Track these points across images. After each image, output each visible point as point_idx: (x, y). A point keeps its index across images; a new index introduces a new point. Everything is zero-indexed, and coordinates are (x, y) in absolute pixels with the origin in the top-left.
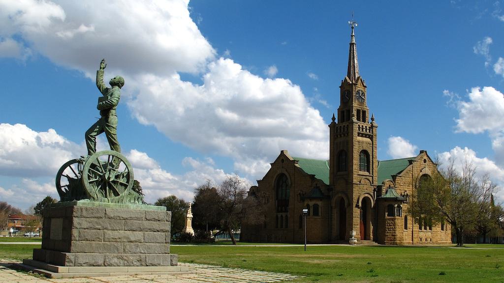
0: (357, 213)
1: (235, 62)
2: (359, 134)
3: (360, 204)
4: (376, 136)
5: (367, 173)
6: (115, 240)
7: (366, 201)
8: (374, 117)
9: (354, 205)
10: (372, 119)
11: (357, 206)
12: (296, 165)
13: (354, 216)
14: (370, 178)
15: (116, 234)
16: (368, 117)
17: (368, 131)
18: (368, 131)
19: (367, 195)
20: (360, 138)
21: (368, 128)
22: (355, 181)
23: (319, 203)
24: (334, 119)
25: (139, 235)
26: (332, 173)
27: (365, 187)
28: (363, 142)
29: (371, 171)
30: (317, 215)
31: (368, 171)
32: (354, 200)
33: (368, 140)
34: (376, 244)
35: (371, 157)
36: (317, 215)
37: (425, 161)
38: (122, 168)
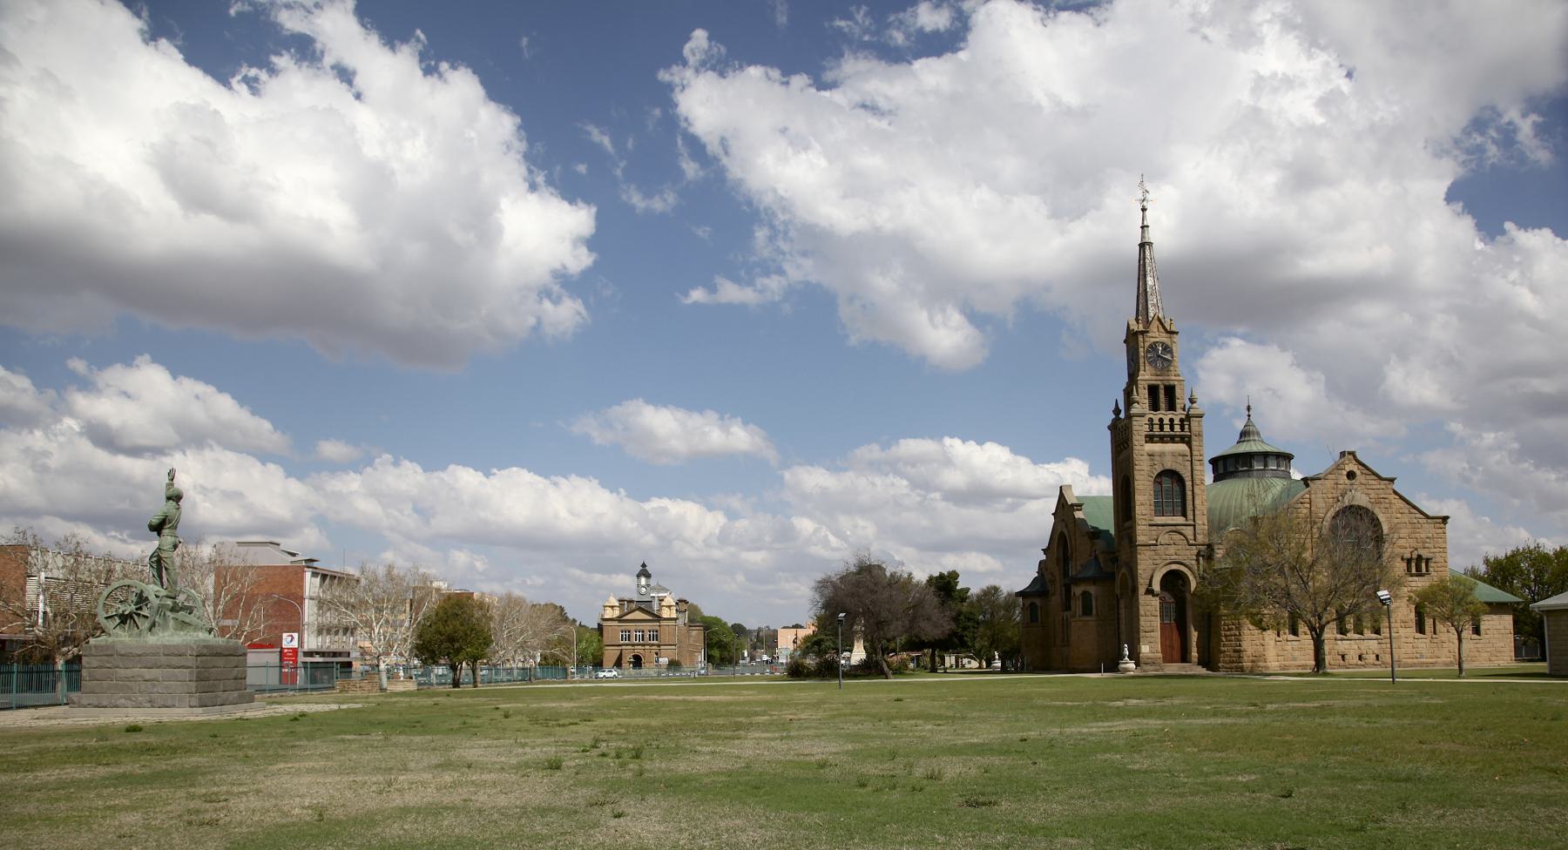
0: (1150, 611)
1: (175, 374)
2: (1150, 439)
3: (1156, 587)
4: (1200, 435)
5: (1181, 520)
6: (128, 679)
7: (1173, 581)
8: (1196, 395)
9: (1142, 590)
10: (1192, 401)
11: (1150, 592)
12: (1079, 515)
13: (1142, 612)
14: (1188, 531)
15: (129, 672)
16: (1182, 399)
17: (1177, 428)
18: (1177, 428)
19: (1174, 567)
20: (1150, 447)
21: (1177, 421)
22: (1141, 539)
23: (1092, 589)
24: (1117, 411)
25: (155, 672)
26: (1117, 525)
27: (1172, 550)
28: (1162, 454)
29: (1190, 514)
30: (1090, 614)
31: (1184, 514)
32: (1140, 581)
33: (1183, 447)
34: (1203, 671)
35: (1188, 484)
36: (1090, 614)
37: (1351, 475)
38: (118, 567)
